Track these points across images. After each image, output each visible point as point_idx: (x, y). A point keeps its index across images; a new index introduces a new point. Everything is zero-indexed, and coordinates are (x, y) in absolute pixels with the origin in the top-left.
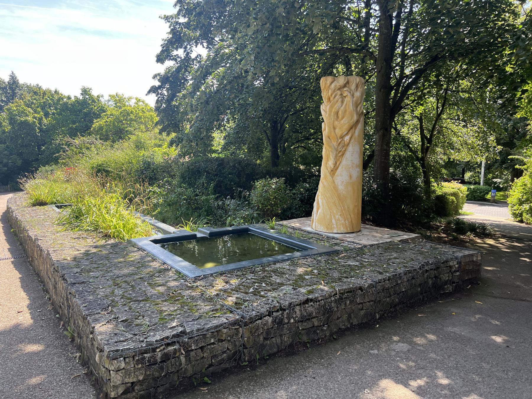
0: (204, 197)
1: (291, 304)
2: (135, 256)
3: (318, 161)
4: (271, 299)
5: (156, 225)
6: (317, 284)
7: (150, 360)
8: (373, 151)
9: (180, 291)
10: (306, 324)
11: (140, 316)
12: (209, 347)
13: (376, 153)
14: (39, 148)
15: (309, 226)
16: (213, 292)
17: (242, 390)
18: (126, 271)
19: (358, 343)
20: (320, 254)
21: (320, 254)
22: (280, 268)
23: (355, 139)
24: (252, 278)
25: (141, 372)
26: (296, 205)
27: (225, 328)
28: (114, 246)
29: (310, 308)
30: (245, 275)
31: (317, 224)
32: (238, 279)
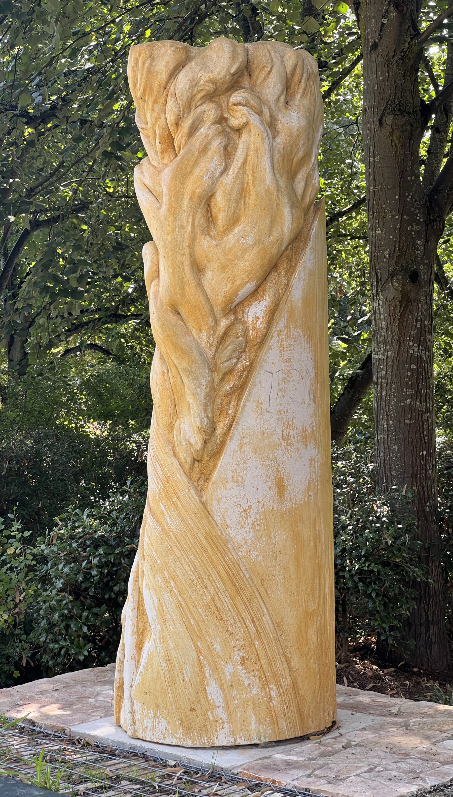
3: (141, 410)
8: (367, 363)
13: (380, 372)
23: (291, 313)
26: (52, 609)
31: (138, 707)
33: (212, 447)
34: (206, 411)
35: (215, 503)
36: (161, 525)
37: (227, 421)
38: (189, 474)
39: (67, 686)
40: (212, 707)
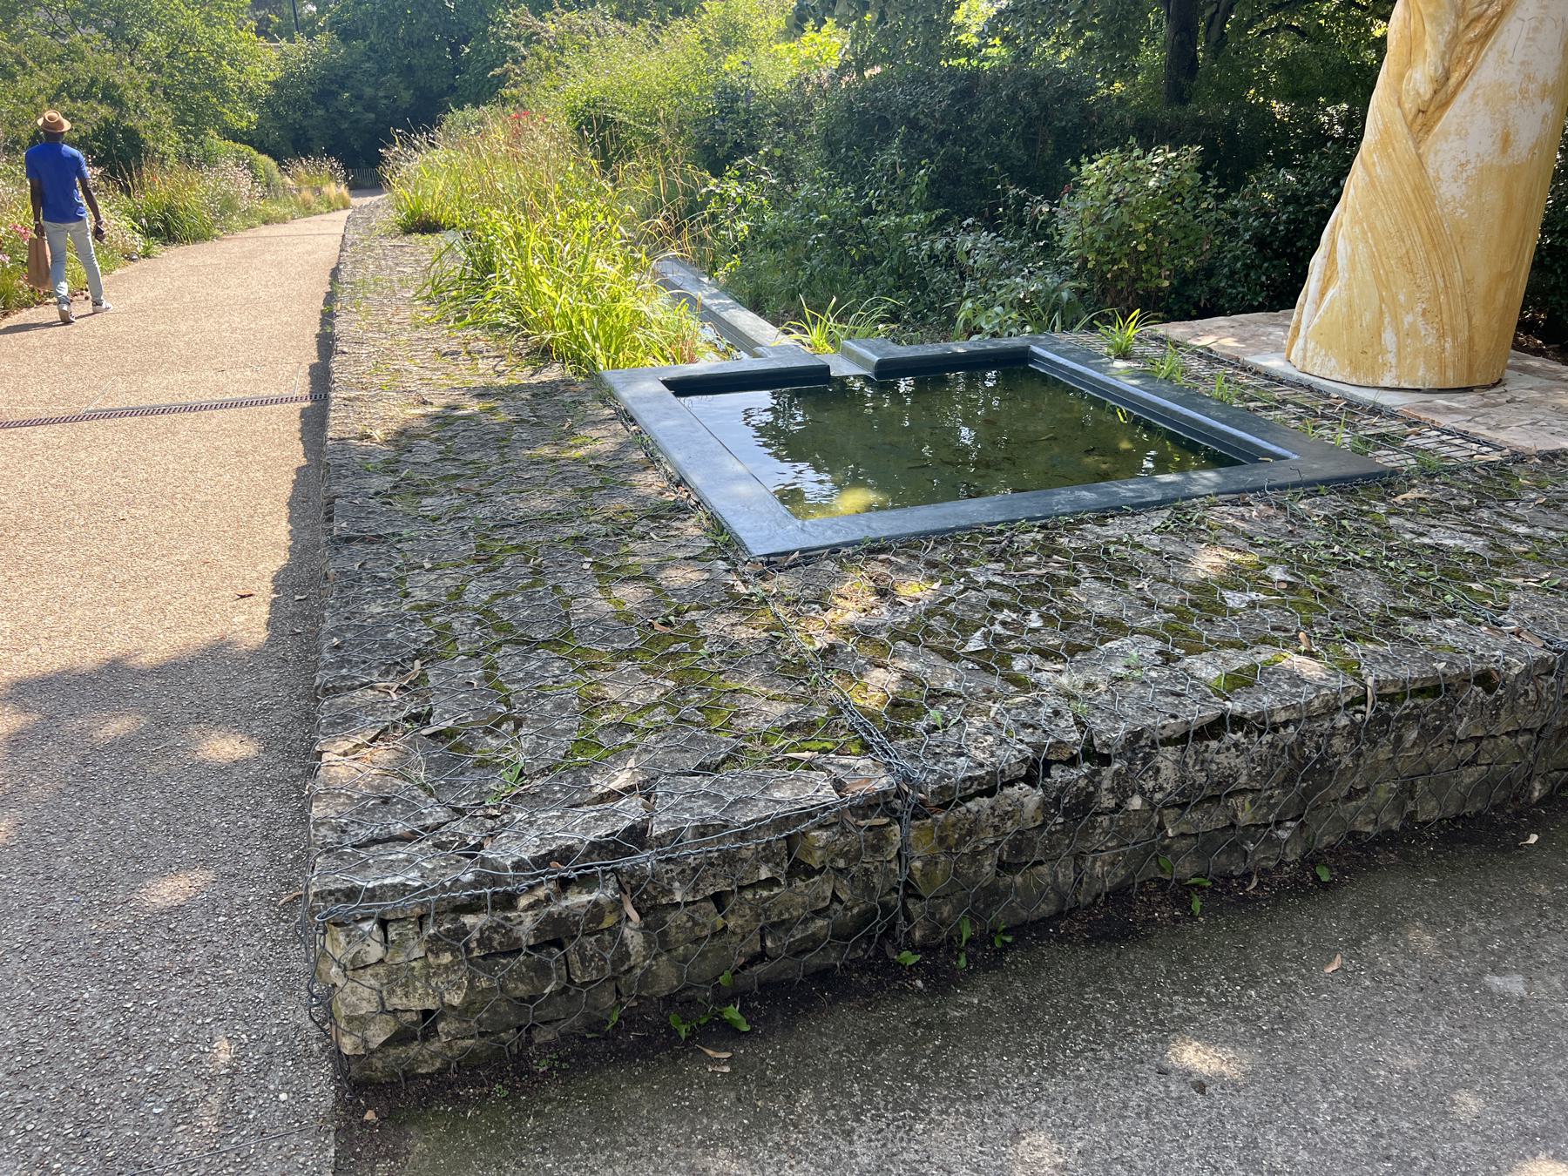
0: (891, 220)
1: (1137, 736)
2: (600, 441)
4: (1051, 700)
5: (725, 315)
6: (1274, 642)
7: (490, 939)
9: (694, 615)
10: (1196, 816)
11: (506, 718)
12: (749, 895)
14: (455, 51)
15: (1278, 348)
16: (815, 634)
17: (868, 1093)
18: (539, 503)
19: (1431, 925)
20: (1311, 488)
21: (1311, 488)
22: (1119, 541)
24: (990, 585)
25: (453, 977)
27: (820, 827)
28: (546, 392)
29: (1224, 756)
30: (968, 562)
31: (1311, 345)
32: (932, 579)
33: (1442, 94)
34: (1443, 59)
35: (1432, 155)
36: (1369, 175)
37: (1464, 71)
38: (1410, 127)
39: (1242, 325)
40: (1383, 352)
